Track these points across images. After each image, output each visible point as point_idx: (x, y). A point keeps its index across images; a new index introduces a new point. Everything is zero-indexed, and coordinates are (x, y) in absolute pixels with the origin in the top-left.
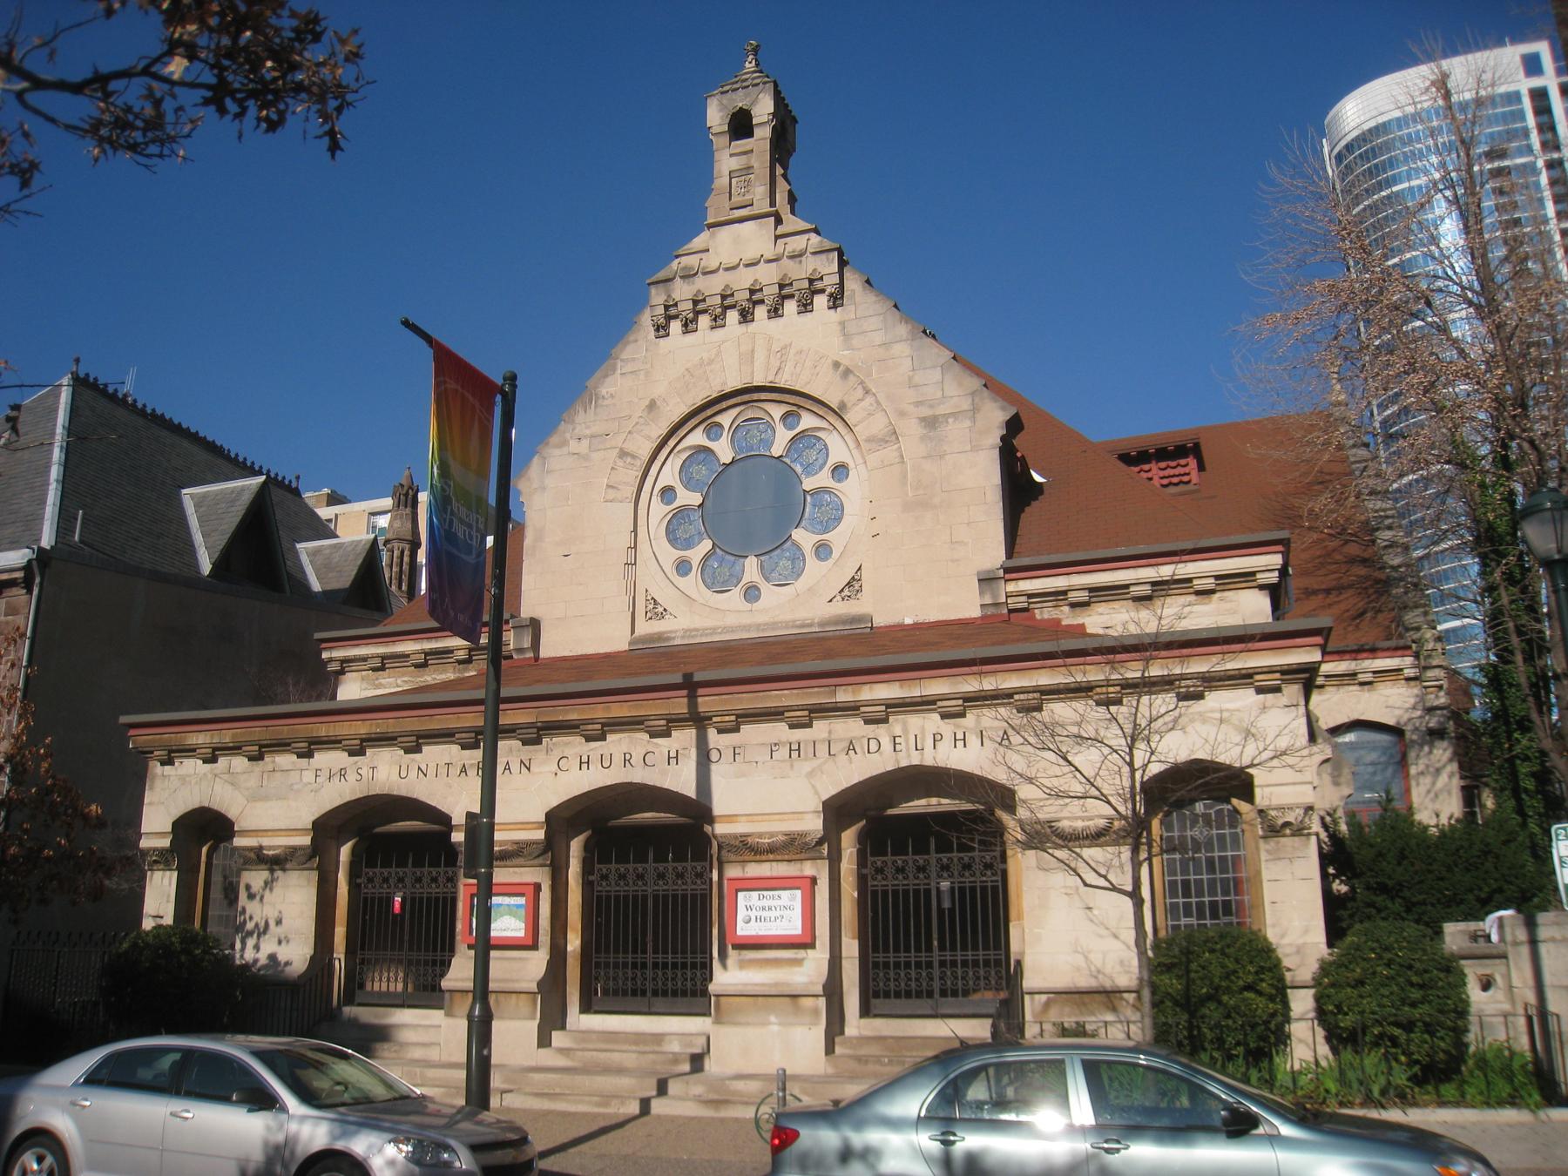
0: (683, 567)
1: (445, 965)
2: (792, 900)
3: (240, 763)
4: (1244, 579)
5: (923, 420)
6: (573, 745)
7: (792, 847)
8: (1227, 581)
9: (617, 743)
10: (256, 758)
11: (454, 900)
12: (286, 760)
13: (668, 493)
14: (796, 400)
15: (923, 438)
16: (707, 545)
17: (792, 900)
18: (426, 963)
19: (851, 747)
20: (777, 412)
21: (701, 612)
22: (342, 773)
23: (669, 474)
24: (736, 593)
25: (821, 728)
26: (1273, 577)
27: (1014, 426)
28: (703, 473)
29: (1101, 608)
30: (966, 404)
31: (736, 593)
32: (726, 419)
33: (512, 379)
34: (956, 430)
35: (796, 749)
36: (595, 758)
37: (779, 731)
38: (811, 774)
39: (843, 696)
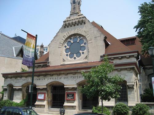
0: (67, 55)
1: (98, 103)
2: (43, 95)
3: (14, 79)
4: (133, 56)
5: (95, 37)
6: (49, 77)
7: (44, 89)
8: (130, 57)
9: (54, 77)
10: (16, 78)
11: (65, 95)
12: (19, 78)
13: (65, 46)
14: (80, 35)
15: (94, 40)
16: (70, 53)
17: (43, 95)
18: (96, 103)
19: (80, 77)
20: (78, 37)
21: (70, 61)
22: (25, 80)
23: (66, 45)
24: (73, 58)
25: (76, 75)
26: (136, 56)
27: (106, 38)
28: (70, 44)
29: (115, 60)
30: (100, 35)
31: (73, 58)
32: (72, 38)
33: (37, 35)
34: (98, 38)
35: (74, 77)
36: (52, 78)
37: (72, 75)
38: (75, 80)
39: (79, 71)
